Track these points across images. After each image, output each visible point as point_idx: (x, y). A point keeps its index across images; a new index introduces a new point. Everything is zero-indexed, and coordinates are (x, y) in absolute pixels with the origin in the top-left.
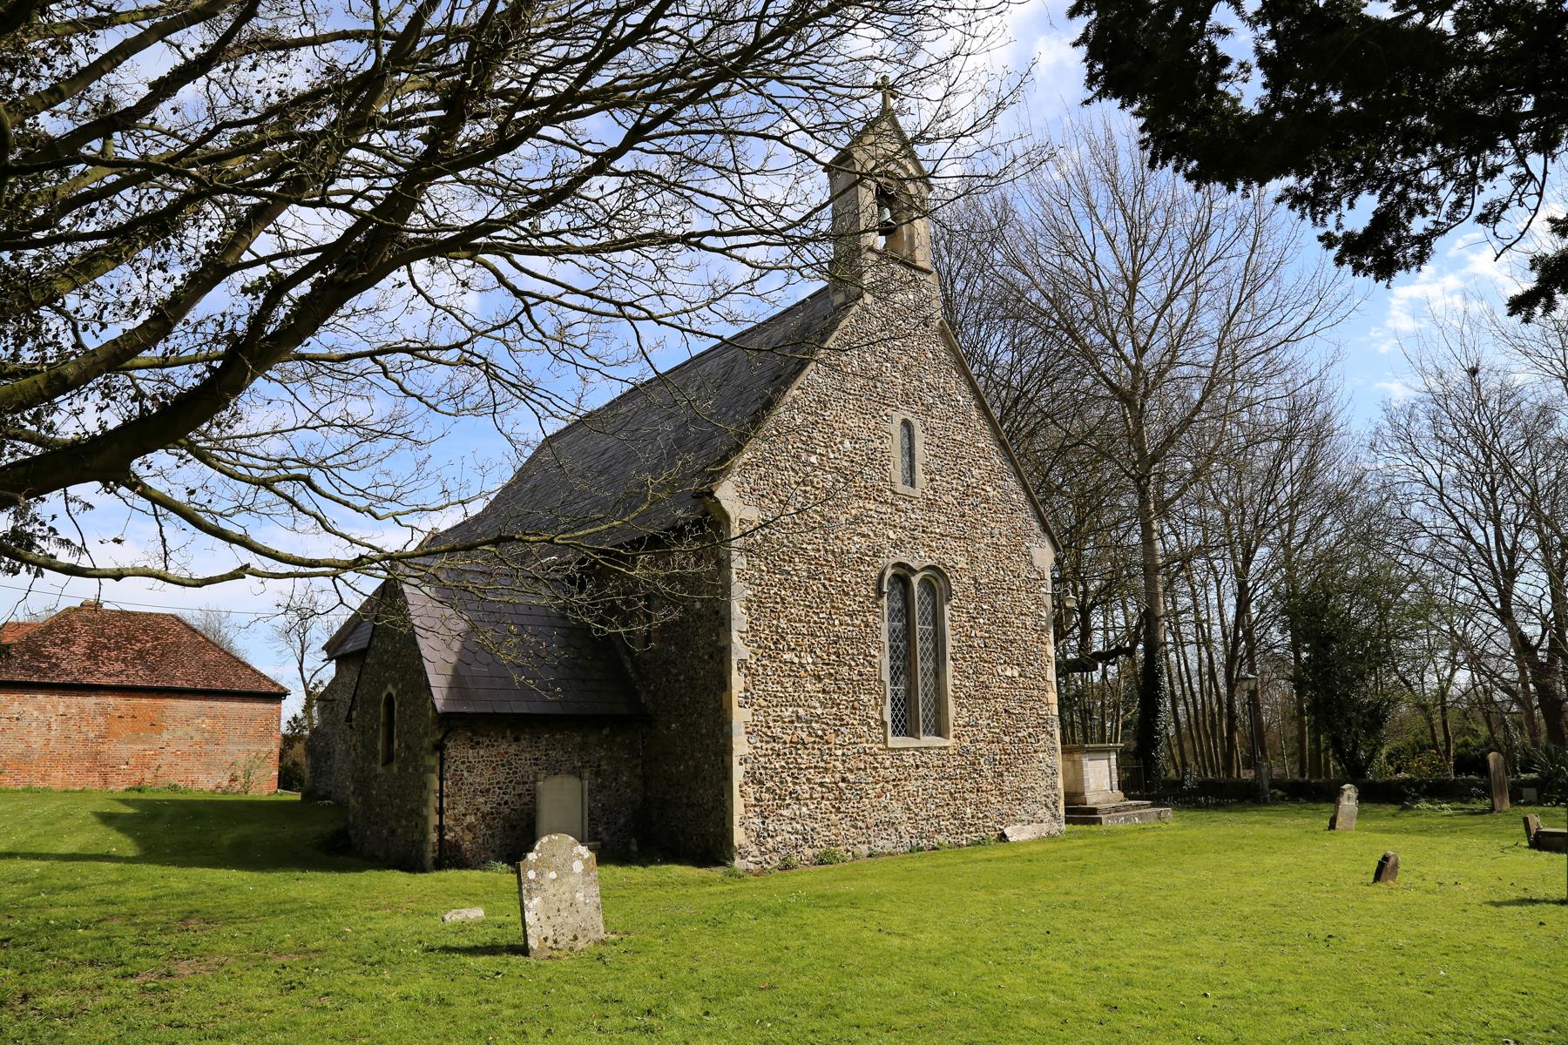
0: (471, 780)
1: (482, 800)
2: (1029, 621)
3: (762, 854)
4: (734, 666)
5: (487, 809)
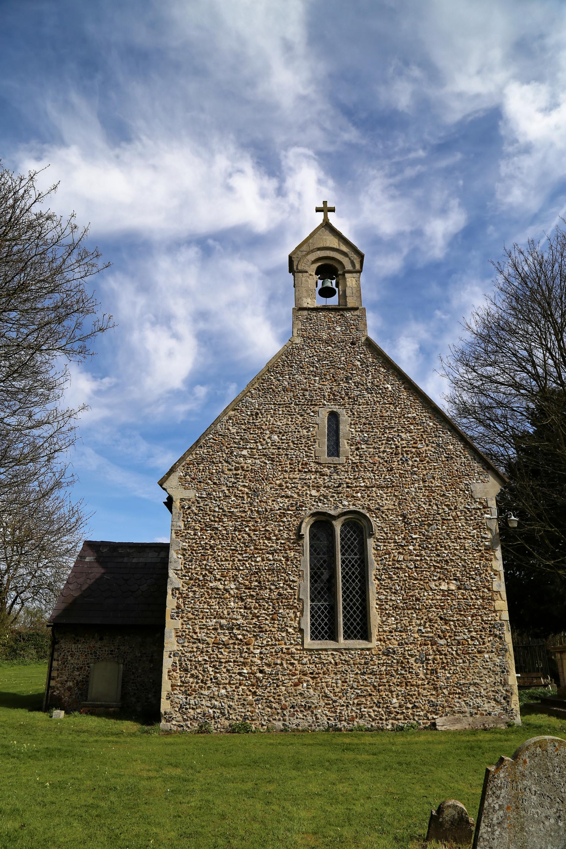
0: (72, 661)
1: (77, 673)
2: (468, 544)
3: (185, 720)
4: (169, 591)
5: (80, 679)
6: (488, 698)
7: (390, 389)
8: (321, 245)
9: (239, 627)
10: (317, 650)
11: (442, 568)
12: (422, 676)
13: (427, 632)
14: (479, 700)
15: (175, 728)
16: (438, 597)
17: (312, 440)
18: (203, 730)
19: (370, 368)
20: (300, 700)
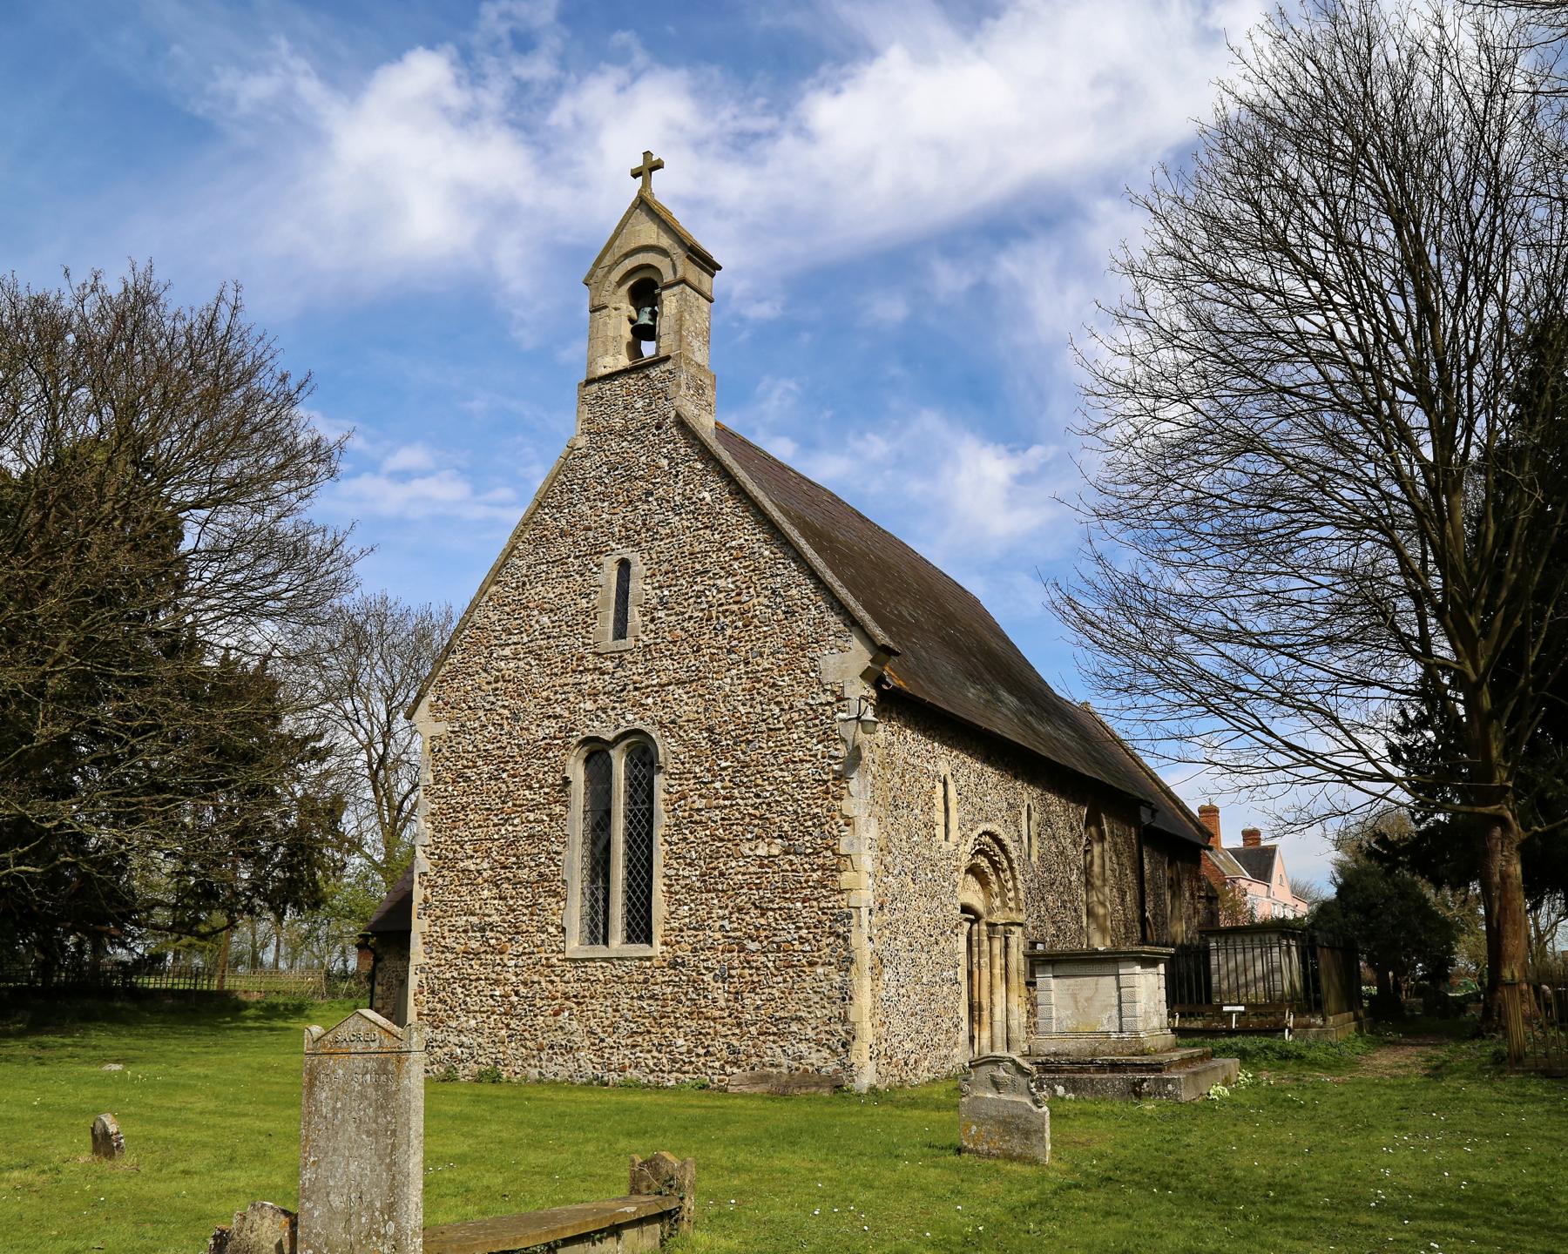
7: (708, 499)
8: (633, 246)
9: (492, 927)
10: (583, 960)
11: (761, 817)
13: (735, 930)
14: (803, 1047)
16: (752, 869)
17: (591, 614)
19: (681, 468)
20: (560, 1038)
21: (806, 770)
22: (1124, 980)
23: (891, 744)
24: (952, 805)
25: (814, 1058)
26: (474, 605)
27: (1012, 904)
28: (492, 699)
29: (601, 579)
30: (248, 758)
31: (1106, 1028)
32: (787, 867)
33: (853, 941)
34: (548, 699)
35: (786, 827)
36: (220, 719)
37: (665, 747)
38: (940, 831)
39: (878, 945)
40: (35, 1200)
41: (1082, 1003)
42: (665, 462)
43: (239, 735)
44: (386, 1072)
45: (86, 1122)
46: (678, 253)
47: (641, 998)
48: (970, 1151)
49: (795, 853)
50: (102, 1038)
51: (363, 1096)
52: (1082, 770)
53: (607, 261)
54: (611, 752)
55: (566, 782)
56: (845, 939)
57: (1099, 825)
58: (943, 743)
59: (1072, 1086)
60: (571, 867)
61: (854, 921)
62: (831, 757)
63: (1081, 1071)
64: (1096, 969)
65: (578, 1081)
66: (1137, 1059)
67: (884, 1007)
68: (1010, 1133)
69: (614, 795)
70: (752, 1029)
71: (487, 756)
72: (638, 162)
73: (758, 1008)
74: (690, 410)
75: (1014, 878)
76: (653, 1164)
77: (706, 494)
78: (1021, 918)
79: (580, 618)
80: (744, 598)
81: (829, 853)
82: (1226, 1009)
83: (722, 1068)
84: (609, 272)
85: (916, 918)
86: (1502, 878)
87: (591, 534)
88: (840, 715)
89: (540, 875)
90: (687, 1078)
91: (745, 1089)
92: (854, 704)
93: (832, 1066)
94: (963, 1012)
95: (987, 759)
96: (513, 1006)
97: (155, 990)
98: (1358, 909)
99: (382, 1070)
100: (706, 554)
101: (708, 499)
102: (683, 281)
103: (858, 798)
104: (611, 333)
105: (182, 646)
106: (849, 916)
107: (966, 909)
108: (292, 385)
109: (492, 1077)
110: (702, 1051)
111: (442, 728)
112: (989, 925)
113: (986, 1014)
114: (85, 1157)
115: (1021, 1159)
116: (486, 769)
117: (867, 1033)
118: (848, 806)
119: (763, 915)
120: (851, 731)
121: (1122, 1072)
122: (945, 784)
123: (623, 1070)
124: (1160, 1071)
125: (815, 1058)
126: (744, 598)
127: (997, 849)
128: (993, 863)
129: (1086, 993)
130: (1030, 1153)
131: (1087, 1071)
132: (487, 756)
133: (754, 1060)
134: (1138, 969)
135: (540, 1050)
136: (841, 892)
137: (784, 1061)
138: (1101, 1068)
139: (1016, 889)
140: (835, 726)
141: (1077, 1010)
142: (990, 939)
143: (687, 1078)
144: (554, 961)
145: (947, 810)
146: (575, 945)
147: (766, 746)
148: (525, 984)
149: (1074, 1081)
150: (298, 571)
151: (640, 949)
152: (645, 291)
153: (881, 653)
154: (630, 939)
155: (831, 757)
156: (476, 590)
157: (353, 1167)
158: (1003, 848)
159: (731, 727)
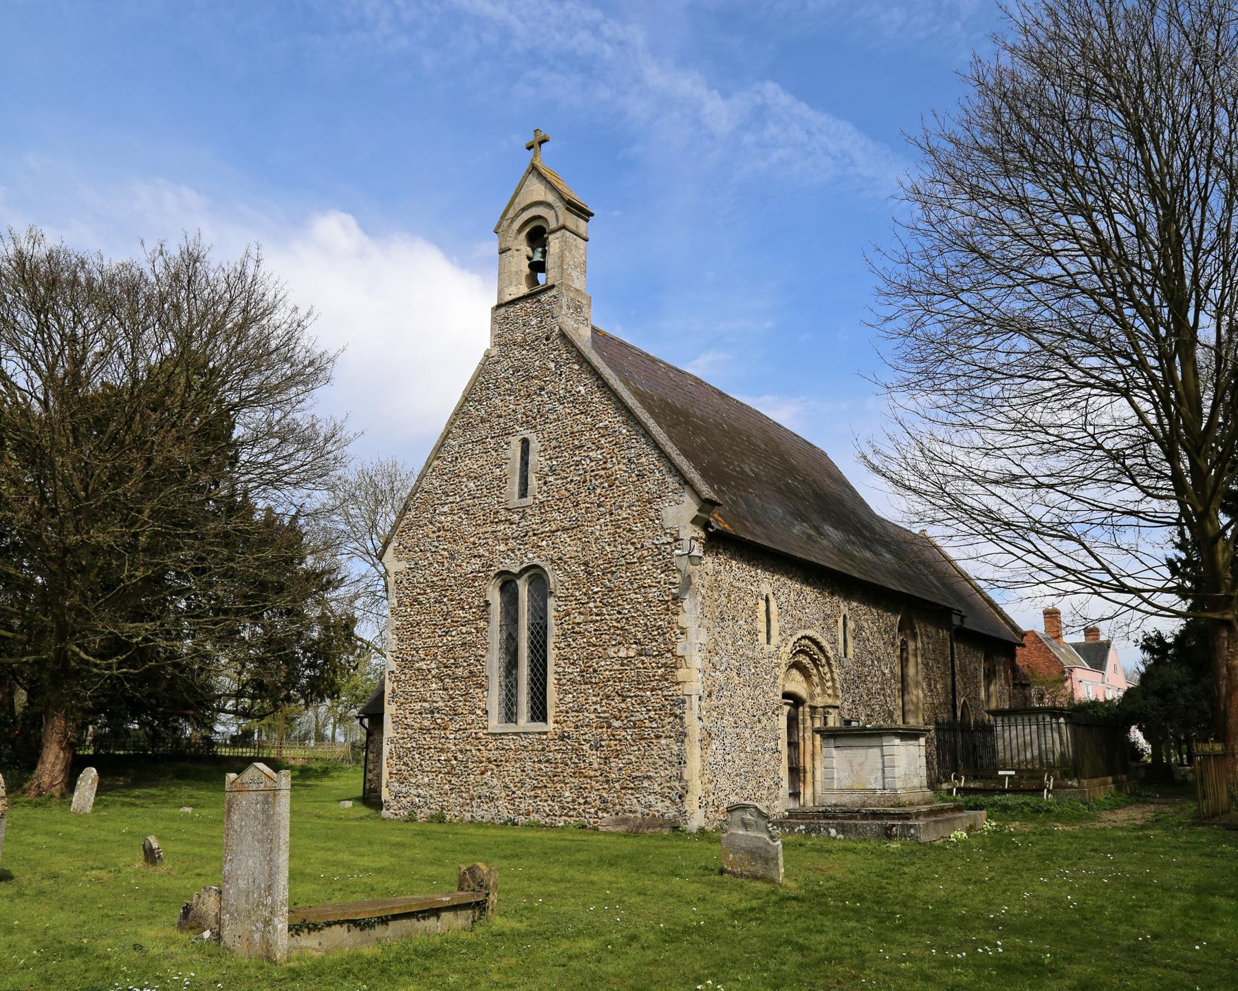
6: (663, 795)
7: (583, 392)
8: (528, 202)
9: (438, 710)
10: (500, 734)
11: (622, 629)
12: (596, 766)
13: (604, 712)
14: (652, 798)
15: (392, 816)
16: (616, 667)
17: (503, 479)
18: (411, 819)
19: (564, 369)
20: (485, 791)
21: (653, 593)
22: (887, 750)
23: (719, 572)
24: (774, 617)
25: (660, 806)
26: (422, 476)
27: (830, 692)
28: (436, 544)
29: (509, 453)
30: (280, 589)
31: (873, 786)
32: (640, 665)
33: (687, 720)
34: (474, 543)
35: (639, 635)
36: (246, 561)
37: (555, 578)
38: (762, 637)
39: (706, 723)
40: (99, 887)
41: (856, 767)
42: (552, 365)
43: (275, 569)
44: (267, 802)
45: (138, 842)
46: (559, 206)
47: (540, 761)
48: (729, 872)
49: (646, 655)
50: (186, 791)
51: (256, 818)
52: (891, 587)
53: (511, 214)
54: (518, 582)
55: (487, 604)
56: (681, 718)
57: (913, 629)
58: (765, 569)
59: (842, 829)
60: (491, 666)
61: (687, 705)
62: (671, 583)
63: (850, 818)
64: (866, 742)
65: (497, 822)
66: (891, 810)
67: (711, 771)
68: (756, 860)
69: (520, 613)
70: (617, 785)
71: (433, 586)
72: (531, 138)
73: (620, 769)
74: (569, 325)
75: (832, 672)
76: (472, 870)
77: (581, 388)
78: (838, 703)
79: (495, 483)
80: (609, 465)
81: (669, 655)
82: (1000, 773)
83: (596, 813)
84: (512, 222)
85: (741, 703)
86: (1228, 670)
87: (502, 420)
88: (677, 552)
89: (471, 672)
90: (571, 820)
91: (610, 828)
92: (686, 543)
93: (672, 813)
94: (784, 773)
95: (806, 581)
96: (453, 768)
97: (229, 757)
98: (1156, 693)
99: (266, 802)
100: (581, 433)
101: (583, 392)
102: (564, 227)
103: (690, 614)
104: (514, 269)
105: (237, 508)
106: (684, 702)
107: (786, 695)
108: (302, 313)
109: (440, 819)
110: (582, 801)
111: (403, 566)
112: (812, 707)
113: (809, 775)
114: (139, 863)
115: (762, 879)
116: (432, 595)
117: (697, 788)
118: (683, 620)
119: (624, 701)
120: (683, 564)
121: (880, 819)
122: (767, 600)
123: (528, 814)
124: (908, 819)
125: (660, 806)
126: (609, 465)
127: (816, 650)
128: (814, 661)
129: (859, 760)
130: (769, 875)
131: (855, 818)
132: (433, 586)
133: (618, 807)
134: (897, 741)
135: (472, 799)
136: (678, 684)
137: (639, 808)
138: (865, 816)
139: (833, 680)
140: (673, 560)
141: (842, 774)
142: (812, 718)
143: (571, 820)
144: (480, 735)
145: (768, 620)
146: (495, 723)
147: (625, 575)
148: (461, 751)
149: (843, 825)
150: (315, 451)
151: (538, 726)
152: (537, 236)
153: (707, 505)
154: (533, 719)
155: (671, 583)
156: (423, 464)
157: (250, 862)
158: (821, 649)
159: (601, 562)
